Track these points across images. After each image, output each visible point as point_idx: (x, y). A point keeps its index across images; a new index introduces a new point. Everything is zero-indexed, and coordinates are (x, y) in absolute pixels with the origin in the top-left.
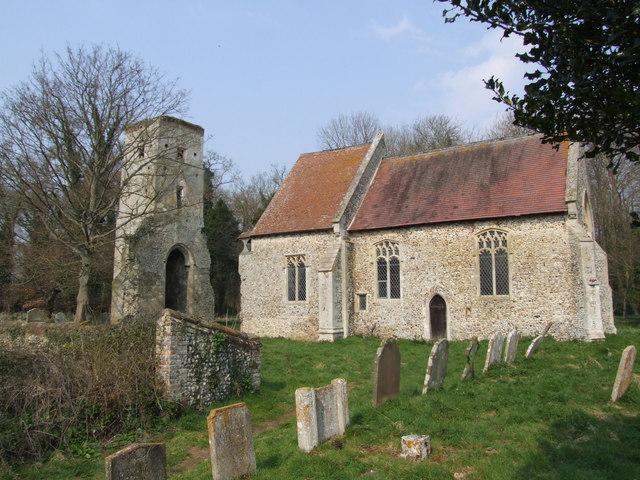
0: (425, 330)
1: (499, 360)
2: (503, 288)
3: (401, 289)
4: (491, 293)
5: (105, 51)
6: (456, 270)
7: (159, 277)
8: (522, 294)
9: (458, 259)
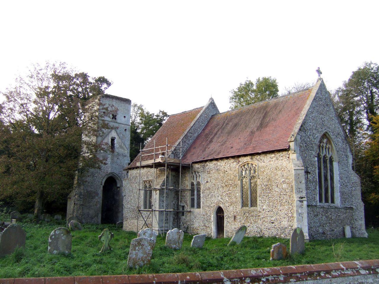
0: (212, 230)
1: (108, 230)
2: (254, 203)
3: (201, 202)
4: (194, 198)
5: (261, 79)
6: (229, 190)
7: (97, 194)
8: (264, 207)
9: (230, 182)
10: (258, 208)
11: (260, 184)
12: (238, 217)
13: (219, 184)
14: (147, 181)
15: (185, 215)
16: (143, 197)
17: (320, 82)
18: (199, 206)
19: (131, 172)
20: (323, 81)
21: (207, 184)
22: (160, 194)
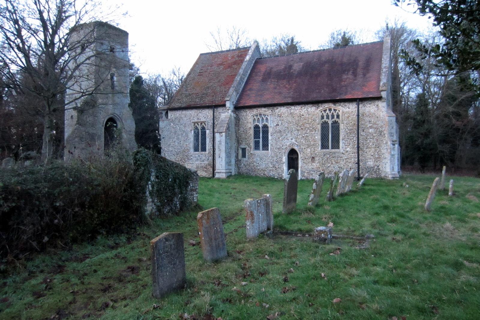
3: (269, 145)
8: (348, 149)
9: (308, 126)
10: (341, 150)
11: (344, 128)
12: (317, 159)
13: (294, 127)
14: (199, 122)
15: (247, 156)
16: (192, 139)
17: (256, 44)
18: (266, 146)
19: (170, 114)
20: (258, 43)
21: (278, 126)
22: (226, 136)
